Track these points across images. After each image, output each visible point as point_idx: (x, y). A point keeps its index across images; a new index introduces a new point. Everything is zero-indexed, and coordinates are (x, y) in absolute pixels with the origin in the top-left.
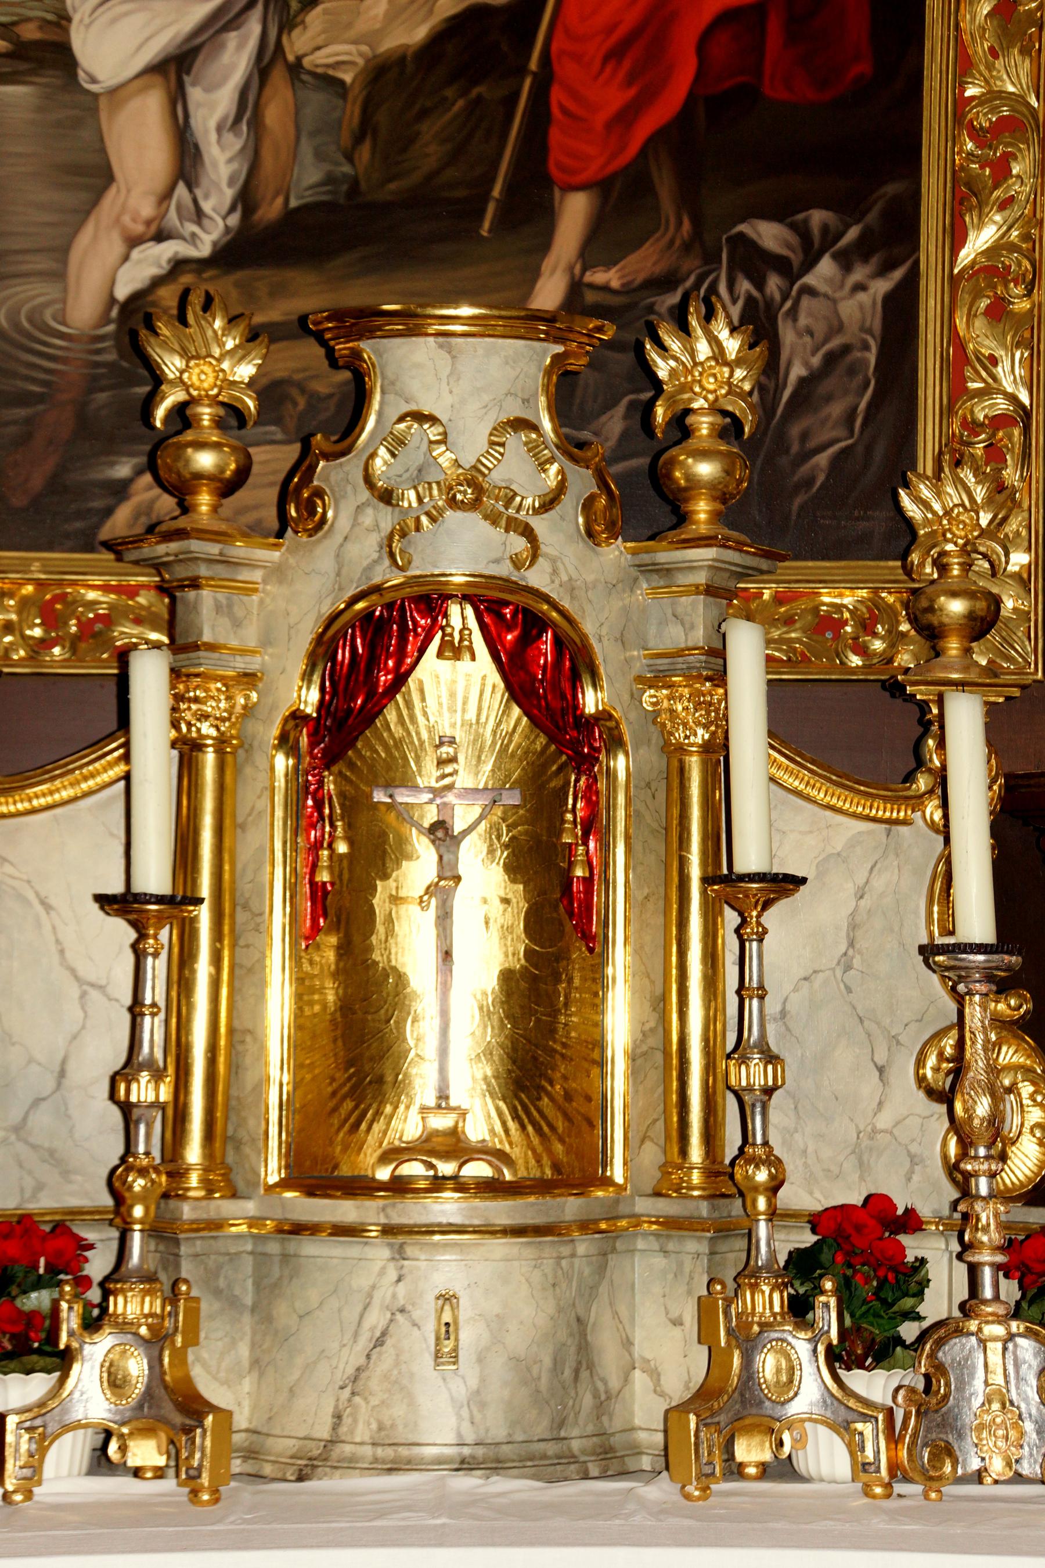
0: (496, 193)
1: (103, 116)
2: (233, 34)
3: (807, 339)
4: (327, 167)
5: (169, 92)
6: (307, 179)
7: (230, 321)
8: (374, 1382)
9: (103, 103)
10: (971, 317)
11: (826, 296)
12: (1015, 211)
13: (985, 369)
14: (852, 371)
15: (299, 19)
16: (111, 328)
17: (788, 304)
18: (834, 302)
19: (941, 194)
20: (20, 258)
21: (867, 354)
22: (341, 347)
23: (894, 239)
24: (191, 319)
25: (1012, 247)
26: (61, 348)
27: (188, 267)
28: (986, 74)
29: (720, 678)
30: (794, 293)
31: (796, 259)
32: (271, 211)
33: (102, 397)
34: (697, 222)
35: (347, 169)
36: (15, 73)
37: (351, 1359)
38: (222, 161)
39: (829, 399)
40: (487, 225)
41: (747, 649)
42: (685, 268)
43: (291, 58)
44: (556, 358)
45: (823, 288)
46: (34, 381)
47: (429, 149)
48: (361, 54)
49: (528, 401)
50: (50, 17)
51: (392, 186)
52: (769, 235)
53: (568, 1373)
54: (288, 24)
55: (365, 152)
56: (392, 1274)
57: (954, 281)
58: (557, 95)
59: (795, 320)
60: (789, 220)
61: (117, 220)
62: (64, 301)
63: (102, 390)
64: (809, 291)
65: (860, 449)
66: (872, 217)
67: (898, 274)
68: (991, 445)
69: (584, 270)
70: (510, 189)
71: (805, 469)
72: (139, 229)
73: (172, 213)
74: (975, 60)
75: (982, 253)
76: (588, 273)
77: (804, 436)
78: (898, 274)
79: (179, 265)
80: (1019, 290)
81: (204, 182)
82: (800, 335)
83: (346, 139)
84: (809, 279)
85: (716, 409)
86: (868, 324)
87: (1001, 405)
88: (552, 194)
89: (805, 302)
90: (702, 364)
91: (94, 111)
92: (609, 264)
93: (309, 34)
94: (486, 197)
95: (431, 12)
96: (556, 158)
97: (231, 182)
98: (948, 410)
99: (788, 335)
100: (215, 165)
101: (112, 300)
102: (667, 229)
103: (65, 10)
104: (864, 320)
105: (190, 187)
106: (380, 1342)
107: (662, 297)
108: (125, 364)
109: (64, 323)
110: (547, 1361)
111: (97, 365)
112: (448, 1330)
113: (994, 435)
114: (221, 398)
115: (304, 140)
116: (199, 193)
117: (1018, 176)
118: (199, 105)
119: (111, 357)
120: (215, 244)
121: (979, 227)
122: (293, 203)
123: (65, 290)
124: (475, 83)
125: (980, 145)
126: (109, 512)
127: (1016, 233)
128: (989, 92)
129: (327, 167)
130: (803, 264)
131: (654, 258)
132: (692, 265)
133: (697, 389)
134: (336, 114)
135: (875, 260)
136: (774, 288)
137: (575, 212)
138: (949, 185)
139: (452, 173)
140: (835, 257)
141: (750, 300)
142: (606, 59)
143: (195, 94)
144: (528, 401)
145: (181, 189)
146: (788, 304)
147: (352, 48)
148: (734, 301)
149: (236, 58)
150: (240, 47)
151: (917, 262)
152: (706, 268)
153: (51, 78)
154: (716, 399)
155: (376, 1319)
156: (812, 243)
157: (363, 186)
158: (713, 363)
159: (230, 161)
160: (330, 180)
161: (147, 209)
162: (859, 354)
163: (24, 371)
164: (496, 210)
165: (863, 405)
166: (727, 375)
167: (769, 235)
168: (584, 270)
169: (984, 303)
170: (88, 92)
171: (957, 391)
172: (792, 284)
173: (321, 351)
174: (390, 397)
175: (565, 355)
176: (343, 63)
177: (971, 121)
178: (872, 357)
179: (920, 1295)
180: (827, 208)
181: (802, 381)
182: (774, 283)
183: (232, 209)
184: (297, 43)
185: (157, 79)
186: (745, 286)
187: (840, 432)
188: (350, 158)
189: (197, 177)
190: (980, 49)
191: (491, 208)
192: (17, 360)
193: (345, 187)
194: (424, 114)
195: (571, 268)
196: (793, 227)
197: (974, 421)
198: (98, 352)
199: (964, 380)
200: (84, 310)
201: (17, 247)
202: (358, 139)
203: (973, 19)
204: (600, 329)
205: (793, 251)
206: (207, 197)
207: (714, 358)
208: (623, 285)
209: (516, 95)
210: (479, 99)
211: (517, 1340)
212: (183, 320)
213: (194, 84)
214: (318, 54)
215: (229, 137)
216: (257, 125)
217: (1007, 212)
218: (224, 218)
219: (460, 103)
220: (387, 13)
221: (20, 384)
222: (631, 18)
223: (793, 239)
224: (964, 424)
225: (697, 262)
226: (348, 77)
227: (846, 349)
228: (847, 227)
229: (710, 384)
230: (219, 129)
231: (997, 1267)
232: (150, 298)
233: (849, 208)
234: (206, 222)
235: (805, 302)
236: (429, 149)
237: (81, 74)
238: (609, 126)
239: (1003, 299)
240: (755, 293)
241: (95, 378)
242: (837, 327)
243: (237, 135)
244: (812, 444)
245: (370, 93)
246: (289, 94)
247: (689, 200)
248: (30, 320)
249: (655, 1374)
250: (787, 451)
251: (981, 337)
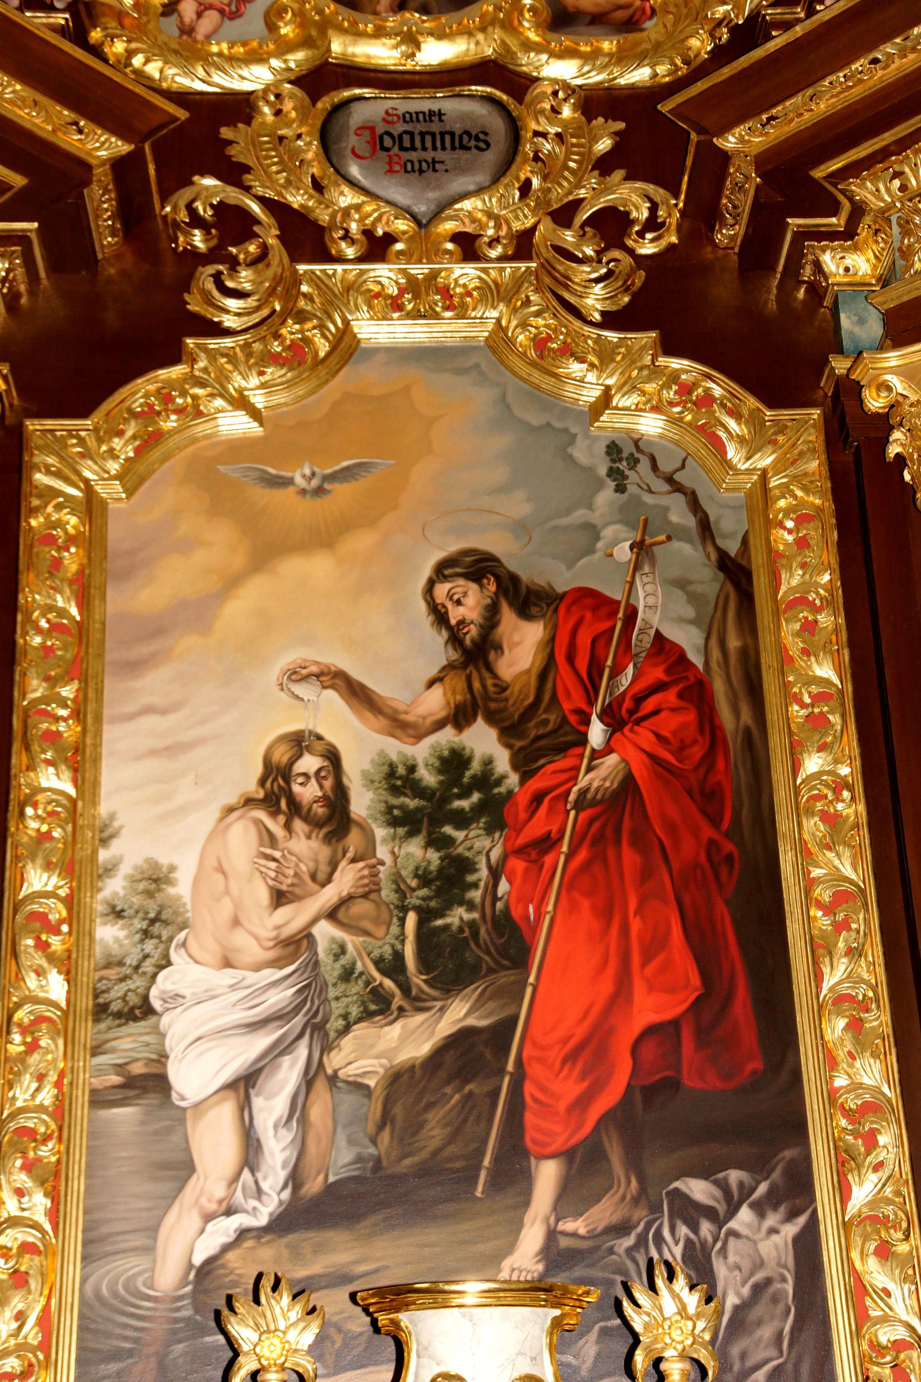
0: (486, 1162)
1: (189, 1123)
2: (287, 1058)
3: (736, 1273)
4: (356, 1150)
5: (239, 1102)
6: (341, 1160)
7: (295, 1297)
9: (189, 1114)
10: (863, 1255)
11: (747, 1238)
12: (884, 1174)
13: (882, 1299)
14: (775, 1300)
15: (335, 1044)
16: (189, 1288)
17: (719, 1245)
18: (755, 1243)
19: (827, 1159)
20: (121, 1238)
21: (785, 1286)
22: (383, 1319)
23: (796, 1192)
24: (263, 1300)
25: (889, 1202)
26: (148, 1309)
27: (250, 1235)
28: (849, 1070)
30: (722, 1235)
31: (721, 1208)
32: (314, 1186)
33: (179, 1348)
34: (641, 1179)
35: (372, 1150)
36: (124, 1099)
38: (277, 1151)
39: (759, 1323)
40: (480, 1187)
42: (635, 1218)
43: (329, 1071)
44: (555, 1319)
46: (126, 1338)
47: (434, 1133)
48: (381, 1066)
49: (535, 1359)
50: (154, 1056)
51: (407, 1162)
52: (699, 1190)
54: (327, 1048)
55: (386, 1135)
57: (846, 1226)
58: (529, 1088)
59: (725, 1257)
60: (713, 1178)
61: (197, 1201)
62: (153, 1270)
63: (180, 1342)
65: (789, 1367)
66: (776, 1175)
67: (802, 1220)
68: (896, 1365)
69: (558, 1221)
70: (496, 1160)
72: (213, 1207)
73: (239, 1193)
74: (839, 1059)
75: (865, 1205)
76: (560, 1223)
77: (743, 1356)
78: (802, 1220)
79: (243, 1234)
80: (900, 1235)
81: (264, 1167)
82: (730, 1269)
83: (371, 1128)
84: (733, 1224)
85: (683, 1356)
86: (783, 1261)
87: (901, 1333)
88: (529, 1162)
89: (732, 1242)
90: (669, 1318)
91: (182, 1121)
92: (577, 1215)
93: (343, 1053)
94: (478, 1167)
95: (433, 1033)
96: (530, 1135)
97: (284, 1167)
98: (857, 1334)
99: (721, 1270)
100: (272, 1154)
101: (190, 1266)
102: (619, 1186)
103: (164, 1050)
104: (779, 1257)
105: (253, 1172)
107: (620, 1241)
108: (198, 1318)
109: (152, 1288)
111: (176, 1320)
113: (897, 1357)
114: (286, 1365)
115: (339, 1130)
116: (259, 1176)
117: (885, 1147)
118: (261, 1110)
119: (187, 1313)
120: (271, 1214)
121: (861, 1183)
122: (331, 1179)
123: (154, 1261)
124: (467, 1082)
125: (852, 1122)
127: (889, 1190)
128: (852, 1083)
129: (356, 1150)
130: (727, 1211)
131: (612, 1208)
132: (641, 1214)
133: (667, 1340)
134: (364, 1110)
135: (782, 1209)
136: (707, 1232)
137: (547, 1176)
138: (832, 1152)
139: (452, 1149)
140: (752, 1206)
141: (688, 1242)
142: (564, 1061)
143: (258, 1102)
144: (535, 1359)
145: (246, 1173)
146: (719, 1245)
147: (375, 1062)
148: (677, 1243)
149: (289, 1073)
150: (292, 1066)
151: (815, 1212)
152: (651, 1217)
153: (152, 1099)
154: (684, 1349)
156: (733, 1196)
157: (385, 1163)
158: (679, 1318)
159: (284, 1149)
160: (359, 1159)
161: (220, 1191)
162: (779, 1286)
163: (118, 1331)
164: (487, 1176)
165: (787, 1329)
166: (691, 1328)
167: (699, 1190)
168: (558, 1221)
169: (872, 1246)
170: (178, 1107)
171: (861, 1317)
172: (720, 1229)
173: (368, 1320)
174: (425, 1361)
175: (563, 1316)
176: (369, 1072)
177: (842, 1104)
178: (789, 1287)
180: (741, 1168)
181: (737, 1309)
182: (706, 1228)
183: (285, 1186)
184: (334, 1061)
185: (230, 1094)
186: (683, 1230)
187: (772, 1352)
188: (374, 1141)
189: (258, 1164)
190: (841, 1054)
191: (483, 1175)
192: (113, 1322)
193: (371, 1164)
194: (430, 1106)
195: (547, 1219)
196: (716, 1183)
197: (879, 1345)
198: (178, 1309)
199: (866, 1309)
200: (168, 1273)
201: (119, 1229)
202: (381, 1127)
203: (833, 1031)
204: (587, 1293)
205: (718, 1202)
206: (265, 1178)
207: (679, 1313)
208: (588, 1232)
209: (498, 1089)
210: (471, 1094)
212: (257, 1301)
213: (257, 1095)
214: (350, 1067)
215: (282, 1132)
216: (304, 1121)
217: (880, 1174)
218: (279, 1194)
219: (457, 1097)
220: (400, 1035)
221: (115, 1343)
222: (580, 1033)
223: (718, 1193)
224: (871, 1345)
225: (645, 1212)
226: (372, 1083)
227: (768, 1281)
228: (758, 1183)
229: (676, 1335)
230: (276, 1127)
232: (220, 1262)
233: (759, 1167)
234: (264, 1198)
235: (732, 1242)
236: (434, 1133)
237: (174, 1095)
238: (570, 1109)
239: (887, 1242)
240: (692, 1236)
241: (174, 1332)
242: (759, 1264)
243: (289, 1130)
244: (750, 1363)
245: (388, 1094)
246: (328, 1096)
247: (635, 1165)
248: (126, 1289)
250: (731, 1369)
251: (876, 1274)
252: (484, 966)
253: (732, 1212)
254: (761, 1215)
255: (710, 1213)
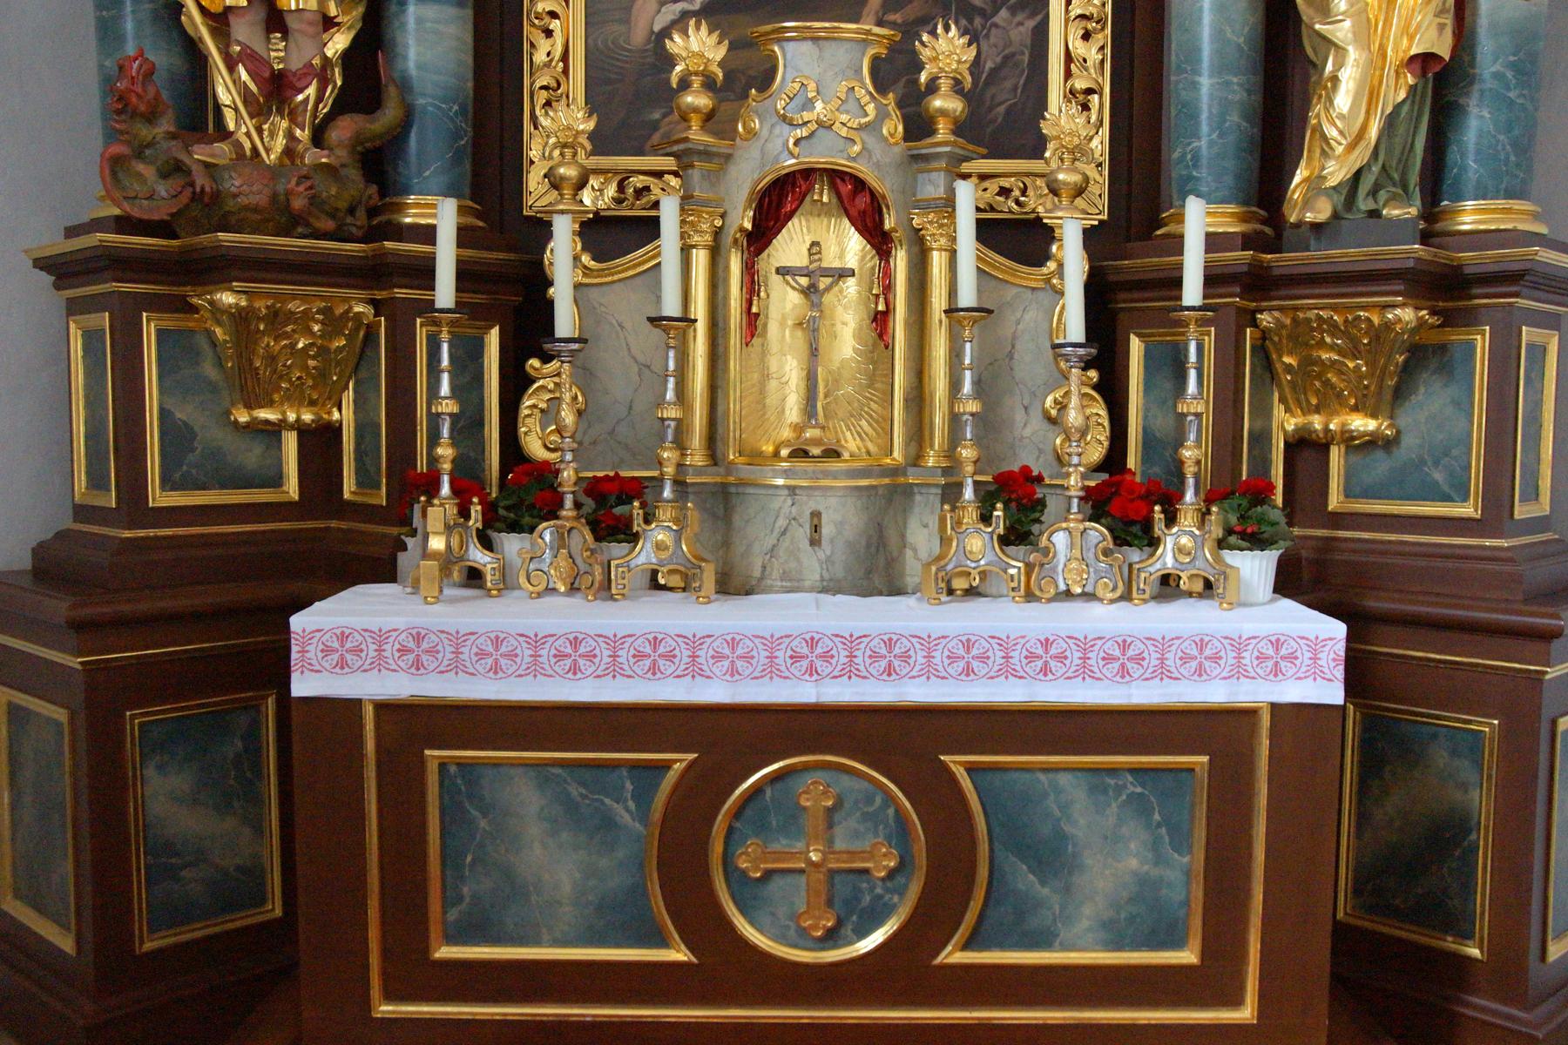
8: (781, 552)
29: (952, 215)
37: (772, 540)
41: (966, 196)
45: (1001, 23)
53: (873, 550)
56: (789, 502)
64: (996, 25)
67: (1039, 18)
71: (992, 115)
77: (993, 97)
78: (1039, 18)
84: (996, 19)
89: (994, 31)
92: (896, 11)
106: (784, 533)
110: (864, 543)
112: (816, 529)
126: (650, 136)
155: (782, 522)
171: (1068, 74)
178: (1026, 59)
179: (1042, 511)
181: (993, 71)
182: (978, 21)
200: (639, 36)
211: (849, 533)
227: (1013, 55)
231: (1081, 499)
235: (994, 31)
242: (1009, 43)
244: (997, 100)
249: (915, 550)
252: (453, 915)
253: (996, 12)
254: (1013, 14)
255: (981, 12)
